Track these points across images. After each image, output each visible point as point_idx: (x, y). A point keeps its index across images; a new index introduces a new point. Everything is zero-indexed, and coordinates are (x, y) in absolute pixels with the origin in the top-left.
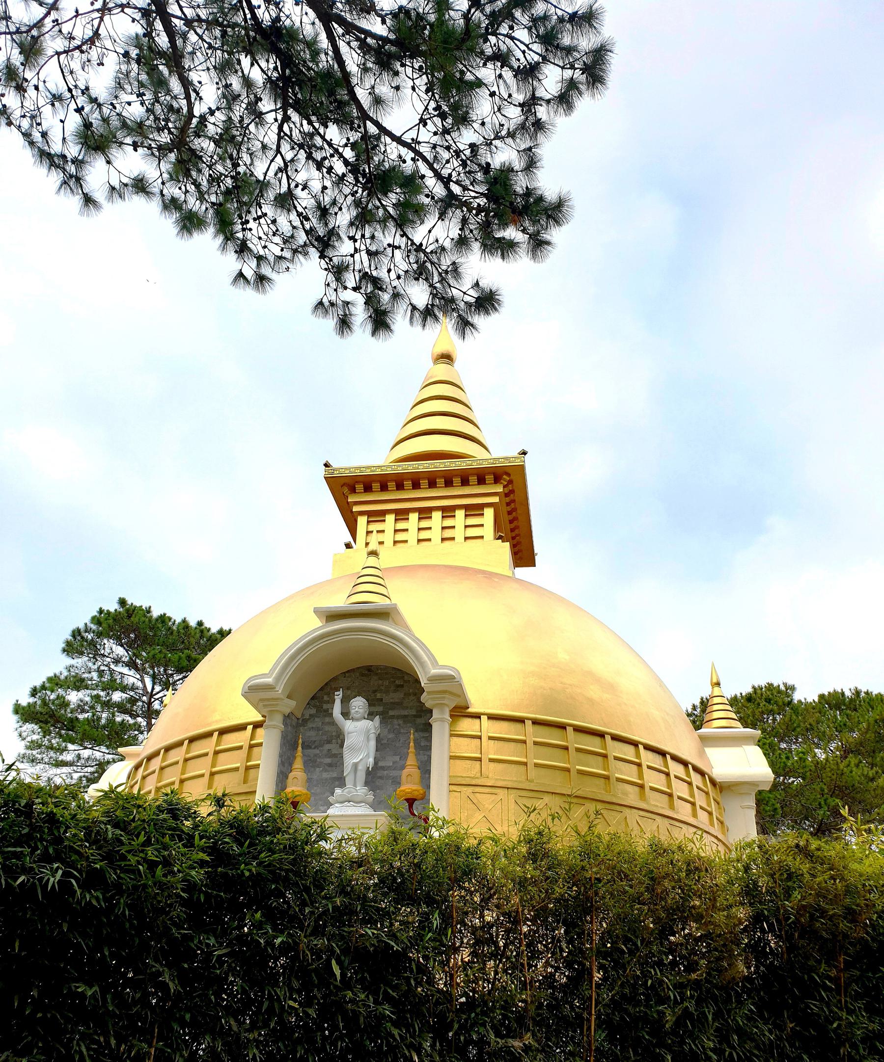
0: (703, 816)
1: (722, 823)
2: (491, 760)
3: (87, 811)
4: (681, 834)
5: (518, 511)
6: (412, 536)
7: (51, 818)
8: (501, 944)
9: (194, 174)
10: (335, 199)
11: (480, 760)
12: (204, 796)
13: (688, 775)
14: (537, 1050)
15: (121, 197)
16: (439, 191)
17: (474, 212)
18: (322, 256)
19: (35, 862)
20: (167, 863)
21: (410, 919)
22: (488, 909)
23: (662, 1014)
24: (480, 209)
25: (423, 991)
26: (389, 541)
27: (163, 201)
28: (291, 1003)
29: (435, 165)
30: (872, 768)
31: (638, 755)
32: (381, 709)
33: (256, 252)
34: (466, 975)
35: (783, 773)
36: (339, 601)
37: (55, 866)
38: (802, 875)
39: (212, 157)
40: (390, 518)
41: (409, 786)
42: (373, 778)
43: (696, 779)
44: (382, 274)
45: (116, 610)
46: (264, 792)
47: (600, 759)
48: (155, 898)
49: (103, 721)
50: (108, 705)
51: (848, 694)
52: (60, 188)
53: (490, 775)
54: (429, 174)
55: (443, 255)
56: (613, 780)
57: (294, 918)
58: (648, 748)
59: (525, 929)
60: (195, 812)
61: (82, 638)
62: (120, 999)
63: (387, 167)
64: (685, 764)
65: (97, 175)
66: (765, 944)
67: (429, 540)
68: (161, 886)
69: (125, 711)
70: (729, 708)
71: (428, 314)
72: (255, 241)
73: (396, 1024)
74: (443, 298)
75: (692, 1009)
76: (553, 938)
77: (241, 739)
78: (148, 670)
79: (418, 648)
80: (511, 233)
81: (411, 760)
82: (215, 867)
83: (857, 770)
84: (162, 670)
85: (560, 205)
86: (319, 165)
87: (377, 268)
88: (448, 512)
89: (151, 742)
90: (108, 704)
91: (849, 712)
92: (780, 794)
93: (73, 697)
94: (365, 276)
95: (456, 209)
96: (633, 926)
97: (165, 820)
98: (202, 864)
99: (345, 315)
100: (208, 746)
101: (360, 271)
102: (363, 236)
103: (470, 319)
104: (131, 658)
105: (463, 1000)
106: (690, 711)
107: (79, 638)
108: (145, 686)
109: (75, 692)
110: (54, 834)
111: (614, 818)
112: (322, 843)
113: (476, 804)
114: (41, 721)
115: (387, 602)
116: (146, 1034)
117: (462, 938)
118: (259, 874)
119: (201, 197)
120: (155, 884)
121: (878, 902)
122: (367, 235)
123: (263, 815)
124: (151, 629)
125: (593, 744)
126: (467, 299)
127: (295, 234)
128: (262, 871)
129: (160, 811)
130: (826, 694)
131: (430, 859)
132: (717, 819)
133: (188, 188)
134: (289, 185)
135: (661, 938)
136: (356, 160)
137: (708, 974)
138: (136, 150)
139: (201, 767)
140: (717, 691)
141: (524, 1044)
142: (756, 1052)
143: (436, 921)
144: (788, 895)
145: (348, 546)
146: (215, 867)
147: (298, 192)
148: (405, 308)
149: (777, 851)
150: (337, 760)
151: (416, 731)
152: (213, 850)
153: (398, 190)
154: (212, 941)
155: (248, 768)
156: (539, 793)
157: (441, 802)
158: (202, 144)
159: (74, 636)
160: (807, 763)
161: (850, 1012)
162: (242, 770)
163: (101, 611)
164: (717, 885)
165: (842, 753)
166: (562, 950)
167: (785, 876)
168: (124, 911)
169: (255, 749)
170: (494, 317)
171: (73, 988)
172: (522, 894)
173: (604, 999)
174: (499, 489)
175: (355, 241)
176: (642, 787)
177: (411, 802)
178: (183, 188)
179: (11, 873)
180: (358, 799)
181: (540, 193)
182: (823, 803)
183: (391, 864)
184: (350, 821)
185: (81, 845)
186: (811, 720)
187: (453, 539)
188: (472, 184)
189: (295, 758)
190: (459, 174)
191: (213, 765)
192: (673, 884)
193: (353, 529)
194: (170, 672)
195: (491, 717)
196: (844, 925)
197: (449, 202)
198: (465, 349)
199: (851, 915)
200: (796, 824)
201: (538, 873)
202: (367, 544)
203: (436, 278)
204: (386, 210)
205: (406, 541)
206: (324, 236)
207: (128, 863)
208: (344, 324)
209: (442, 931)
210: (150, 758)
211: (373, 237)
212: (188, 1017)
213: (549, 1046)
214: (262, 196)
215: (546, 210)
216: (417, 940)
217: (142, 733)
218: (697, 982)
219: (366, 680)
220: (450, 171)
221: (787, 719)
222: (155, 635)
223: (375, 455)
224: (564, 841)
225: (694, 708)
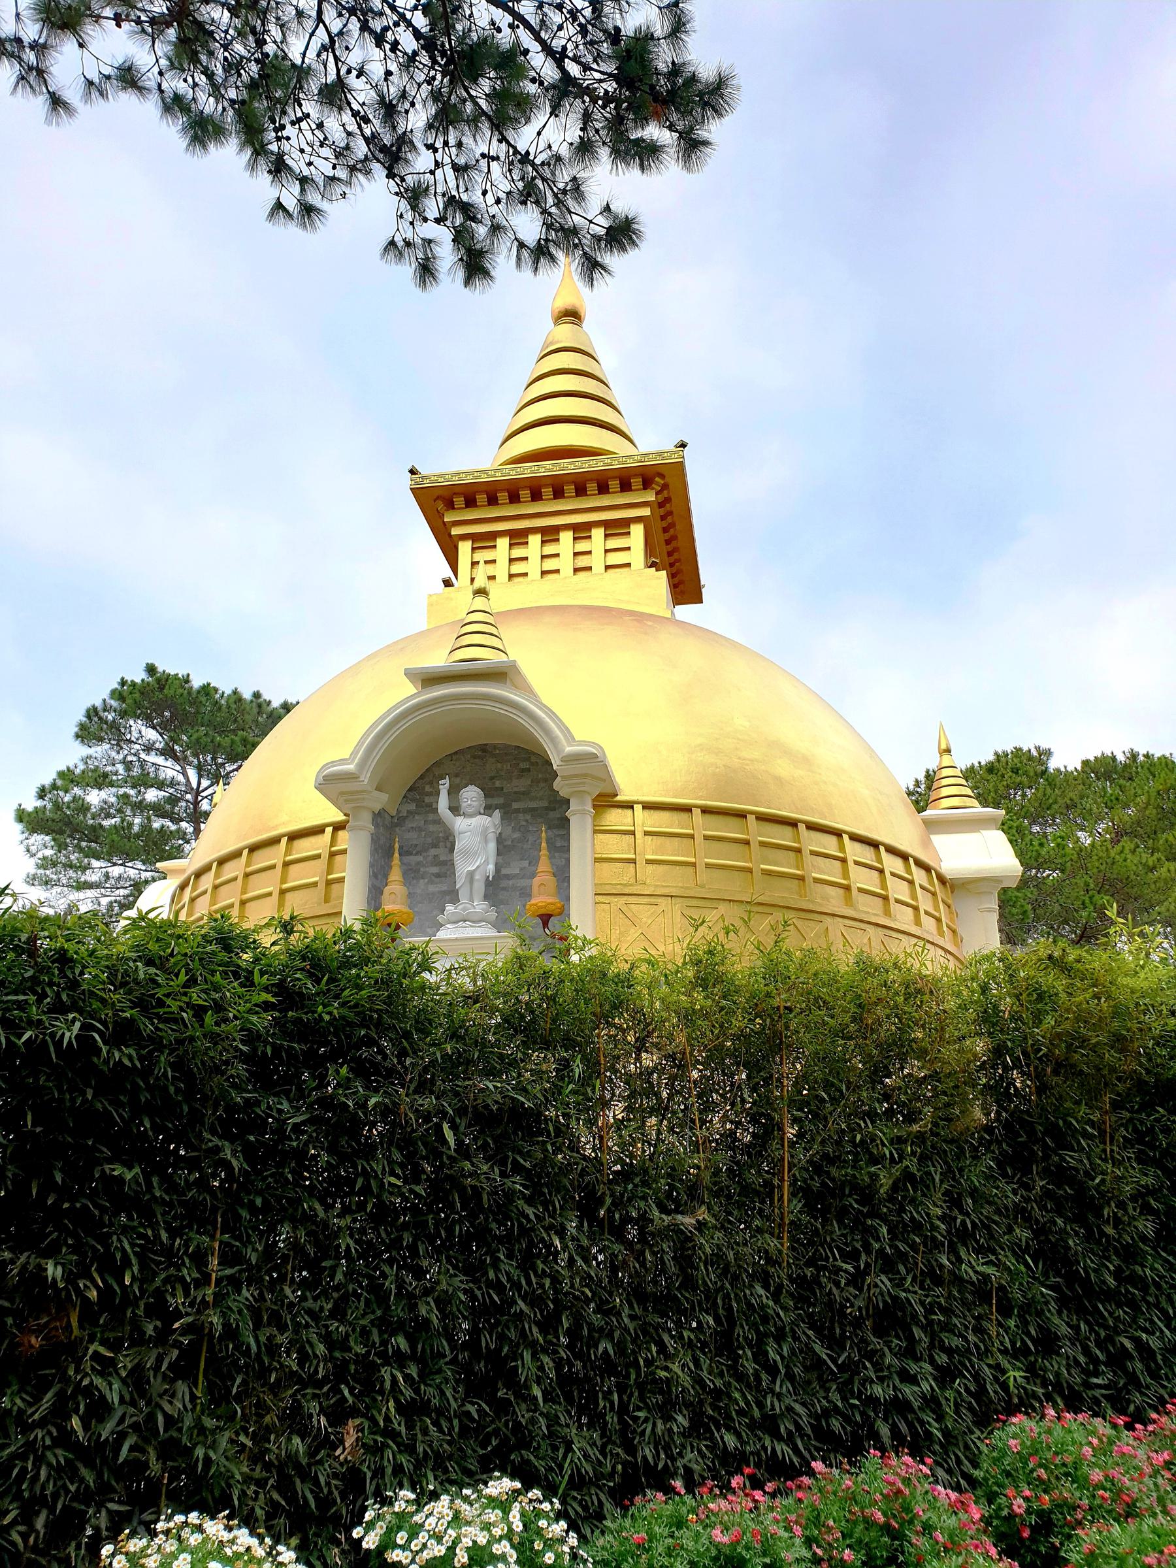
0: (928, 923)
1: (954, 931)
2: (649, 862)
3: (114, 941)
4: (900, 947)
5: (678, 527)
6: (533, 567)
7: (63, 958)
8: (665, 1095)
9: (203, 58)
10: (404, 91)
11: (634, 861)
12: (266, 921)
13: (909, 871)
14: (715, 1227)
15: (101, 94)
16: (550, 73)
17: (600, 102)
18: (391, 175)
19: (44, 1013)
20: (219, 1007)
21: (544, 1067)
22: (647, 1051)
23: (874, 1177)
24: (608, 99)
25: (564, 1158)
26: (502, 576)
27: (163, 100)
28: (393, 1180)
29: (543, 34)
30: (1152, 855)
31: (842, 848)
32: (500, 801)
33: (298, 172)
34: (620, 1136)
35: (1035, 864)
36: (438, 658)
37: (71, 1016)
38: (1056, 994)
39: (226, 32)
40: (503, 543)
41: (542, 899)
42: (495, 889)
43: (919, 876)
44: (476, 197)
45: (143, 680)
46: (352, 909)
48: (206, 1054)
49: (136, 829)
50: (140, 807)
51: (1121, 758)
52: (18, 82)
53: (648, 882)
54: (534, 46)
55: (558, 168)
56: (809, 881)
57: (391, 1073)
58: (855, 838)
59: (695, 1074)
60: (254, 942)
61: (100, 718)
62: (170, 1185)
63: (475, 39)
64: (904, 857)
65: (68, 64)
66: (1009, 1084)
67: (557, 571)
68: (215, 1038)
69: (163, 815)
70: (963, 782)
71: (541, 253)
72: (296, 154)
73: (530, 1201)
74: (562, 228)
75: (914, 1169)
76: (732, 1085)
78: (191, 759)
79: (548, 720)
80: (654, 132)
81: (544, 865)
82: (283, 1011)
83: (1132, 858)
84: (209, 758)
85: (719, 87)
86: (379, 40)
87: (467, 190)
88: (581, 531)
89: (202, 851)
90: (139, 806)
91: (1122, 782)
92: (1031, 893)
93: (94, 798)
94: (452, 202)
95: (575, 98)
96: (835, 1065)
97: (213, 953)
98: (266, 1006)
99: (427, 259)
100: (276, 856)
101: (444, 195)
102: (446, 143)
103: (599, 259)
104: (166, 743)
105: (618, 1167)
106: (911, 788)
107: (96, 719)
108: (188, 780)
109: (96, 792)
110: (65, 976)
111: (812, 931)
112: (426, 975)
113: (628, 918)
114: (53, 831)
115: (503, 658)
116: (205, 1224)
117: (612, 1089)
118: (343, 1018)
119: (216, 91)
120: (205, 1036)
121: (1155, 1025)
122: (452, 142)
123: (345, 942)
124: (191, 704)
125: (783, 836)
126: (596, 230)
127: (352, 144)
128: (345, 1011)
129: (207, 942)
130: (1092, 759)
131: (568, 989)
132: (948, 926)
133: (197, 80)
134: (338, 70)
135: (873, 1082)
136: (431, 30)
137: (935, 1124)
138: (119, 25)
139: (267, 884)
140: (946, 760)
141: (698, 1221)
142: (996, 1218)
143: (578, 1068)
144: (1038, 1019)
145: (447, 583)
146: (283, 1011)
147: (352, 80)
148: (509, 244)
149: (1024, 965)
150: (446, 869)
151: (549, 828)
152: (280, 988)
153: (492, 75)
154: (285, 1106)
155: (329, 883)
156: (711, 901)
157: (583, 919)
158: (213, 14)
159: (88, 716)
160: (1067, 850)
161: (1117, 1163)
162: (322, 885)
163: (123, 682)
164: (945, 1012)
165: (1113, 835)
166: (743, 1101)
167: (1035, 996)
168: (166, 1071)
169: (338, 858)
170: (632, 254)
171: (108, 1172)
172: (689, 1030)
173: (800, 1160)
174: (650, 496)
175: (435, 150)
176: (847, 888)
177: (545, 919)
178: (190, 79)
179: (13, 1027)
180: (476, 918)
181: (692, 69)
182: (1087, 901)
183: (517, 998)
184: (464, 946)
185: (104, 989)
186: (1071, 795)
187: (589, 569)
188: (595, 60)
189: (391, 867)
190: (577, 46)
191: (284, 881)
192: (888, 1011)
193: (452, 560)
194: (220, 761)
195: (647, 806)
196: (1110, 1056)
197: (565, 90)
198: (594, 300)
199: (1120, 1042)
200: (1054, 931)
201: (709, 1002)
202: (473, 580)
203: (550, 201)
204: (476, 104)
205: (526, 575)
206: (392, 145)
207: (166, 1010)
208: (426, 271)
209: (586, 1081)
210: (198, 874)
211: (459, 145)
212: (259, 1201)
213: (730, 1222)
214: (301, 88)
215: (701, 94)
216: (554, 1093)
217: (188, 842)
218: (921, 1137)
219: (479, 762)
220: (563, 42)
221: (1040, 795)
222: (197, 712)
223: (479, 456)
224: (743, 961)
225: (917, 783)
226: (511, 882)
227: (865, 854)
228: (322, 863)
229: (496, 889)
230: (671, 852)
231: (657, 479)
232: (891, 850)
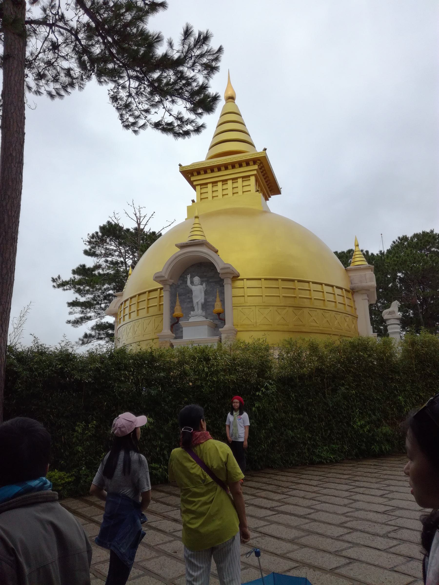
32: (206, 279)
36: (185, 240)
41: (218, 307)
51: (421, 233)
77: (155, 294)
81: (218, 299)
155: (160, 305)
162: (158, 306)
174: (256, 167)
177: (219, 314)
189: (176, 299)
210: (125, 301)
228: (157, 300)
229: (205, 306)
231: (258, 161)
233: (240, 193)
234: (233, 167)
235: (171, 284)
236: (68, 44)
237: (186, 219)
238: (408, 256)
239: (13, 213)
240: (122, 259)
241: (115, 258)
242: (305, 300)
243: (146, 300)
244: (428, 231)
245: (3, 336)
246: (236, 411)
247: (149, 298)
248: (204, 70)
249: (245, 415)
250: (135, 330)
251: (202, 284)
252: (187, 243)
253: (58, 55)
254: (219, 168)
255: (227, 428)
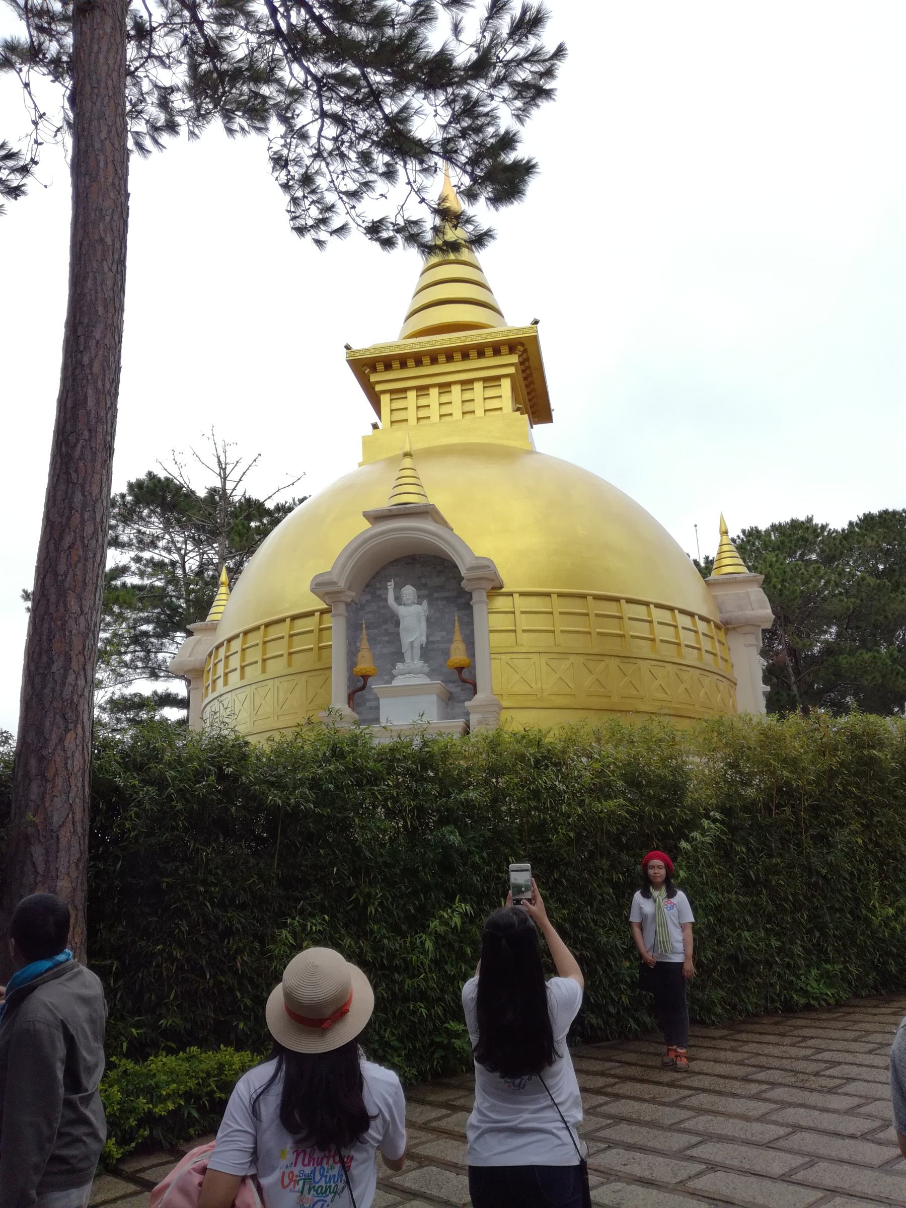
36: (382, 501)
41: (458, 654)
42: (426, 653)
47: (617, 620)
100: (282, 630)
125: (610, 609)
145: (375, 426)
150: (395, 638)
174: (514, 359)
177: (460, 669)
219: (410, 569)
226: (435, 646)
227: (666, 616)
228: (314, 636)
230: (538, 623)
232: (682, 612)
233: (480, 412)
234: (465, 356)
235: (349, 600)
236: (173, 30)
237: (360, 465)
238: (771, 566)
239: (107, 385)
240: (176, 557)
241: (157, 555)
242: (640, 641)
243: (287, 638)
244: (802, 518)
245: (86, 694)
246: (657, 887)
247: (267, 639)
248: (516, 98)
249: (681, 896)
250: (257, 705)
251: (420, 603)
252: (390, 510)
253: (150, 52)
254: (434, 357)
255: (637, 930)
